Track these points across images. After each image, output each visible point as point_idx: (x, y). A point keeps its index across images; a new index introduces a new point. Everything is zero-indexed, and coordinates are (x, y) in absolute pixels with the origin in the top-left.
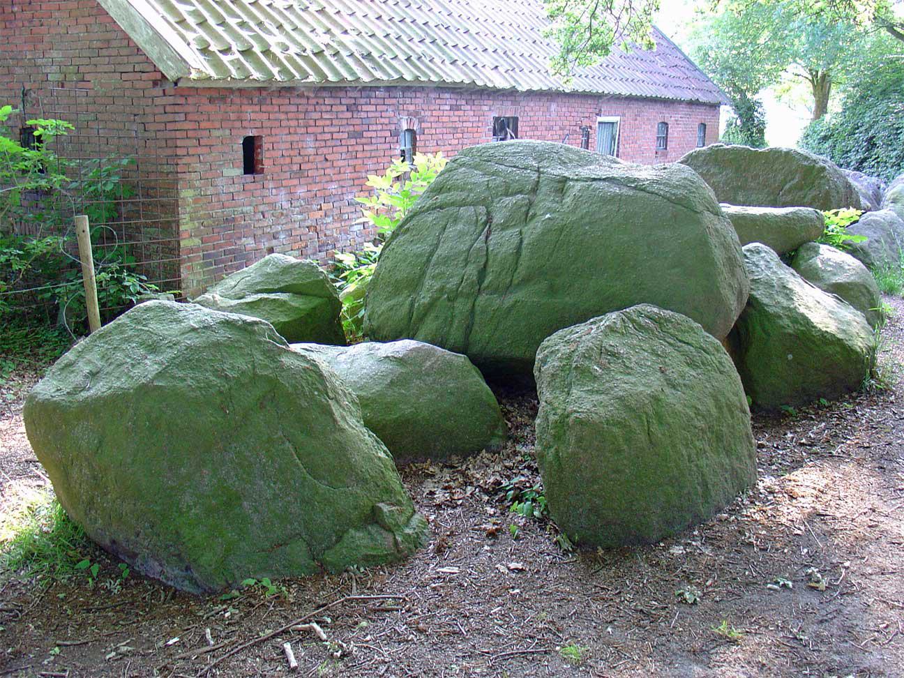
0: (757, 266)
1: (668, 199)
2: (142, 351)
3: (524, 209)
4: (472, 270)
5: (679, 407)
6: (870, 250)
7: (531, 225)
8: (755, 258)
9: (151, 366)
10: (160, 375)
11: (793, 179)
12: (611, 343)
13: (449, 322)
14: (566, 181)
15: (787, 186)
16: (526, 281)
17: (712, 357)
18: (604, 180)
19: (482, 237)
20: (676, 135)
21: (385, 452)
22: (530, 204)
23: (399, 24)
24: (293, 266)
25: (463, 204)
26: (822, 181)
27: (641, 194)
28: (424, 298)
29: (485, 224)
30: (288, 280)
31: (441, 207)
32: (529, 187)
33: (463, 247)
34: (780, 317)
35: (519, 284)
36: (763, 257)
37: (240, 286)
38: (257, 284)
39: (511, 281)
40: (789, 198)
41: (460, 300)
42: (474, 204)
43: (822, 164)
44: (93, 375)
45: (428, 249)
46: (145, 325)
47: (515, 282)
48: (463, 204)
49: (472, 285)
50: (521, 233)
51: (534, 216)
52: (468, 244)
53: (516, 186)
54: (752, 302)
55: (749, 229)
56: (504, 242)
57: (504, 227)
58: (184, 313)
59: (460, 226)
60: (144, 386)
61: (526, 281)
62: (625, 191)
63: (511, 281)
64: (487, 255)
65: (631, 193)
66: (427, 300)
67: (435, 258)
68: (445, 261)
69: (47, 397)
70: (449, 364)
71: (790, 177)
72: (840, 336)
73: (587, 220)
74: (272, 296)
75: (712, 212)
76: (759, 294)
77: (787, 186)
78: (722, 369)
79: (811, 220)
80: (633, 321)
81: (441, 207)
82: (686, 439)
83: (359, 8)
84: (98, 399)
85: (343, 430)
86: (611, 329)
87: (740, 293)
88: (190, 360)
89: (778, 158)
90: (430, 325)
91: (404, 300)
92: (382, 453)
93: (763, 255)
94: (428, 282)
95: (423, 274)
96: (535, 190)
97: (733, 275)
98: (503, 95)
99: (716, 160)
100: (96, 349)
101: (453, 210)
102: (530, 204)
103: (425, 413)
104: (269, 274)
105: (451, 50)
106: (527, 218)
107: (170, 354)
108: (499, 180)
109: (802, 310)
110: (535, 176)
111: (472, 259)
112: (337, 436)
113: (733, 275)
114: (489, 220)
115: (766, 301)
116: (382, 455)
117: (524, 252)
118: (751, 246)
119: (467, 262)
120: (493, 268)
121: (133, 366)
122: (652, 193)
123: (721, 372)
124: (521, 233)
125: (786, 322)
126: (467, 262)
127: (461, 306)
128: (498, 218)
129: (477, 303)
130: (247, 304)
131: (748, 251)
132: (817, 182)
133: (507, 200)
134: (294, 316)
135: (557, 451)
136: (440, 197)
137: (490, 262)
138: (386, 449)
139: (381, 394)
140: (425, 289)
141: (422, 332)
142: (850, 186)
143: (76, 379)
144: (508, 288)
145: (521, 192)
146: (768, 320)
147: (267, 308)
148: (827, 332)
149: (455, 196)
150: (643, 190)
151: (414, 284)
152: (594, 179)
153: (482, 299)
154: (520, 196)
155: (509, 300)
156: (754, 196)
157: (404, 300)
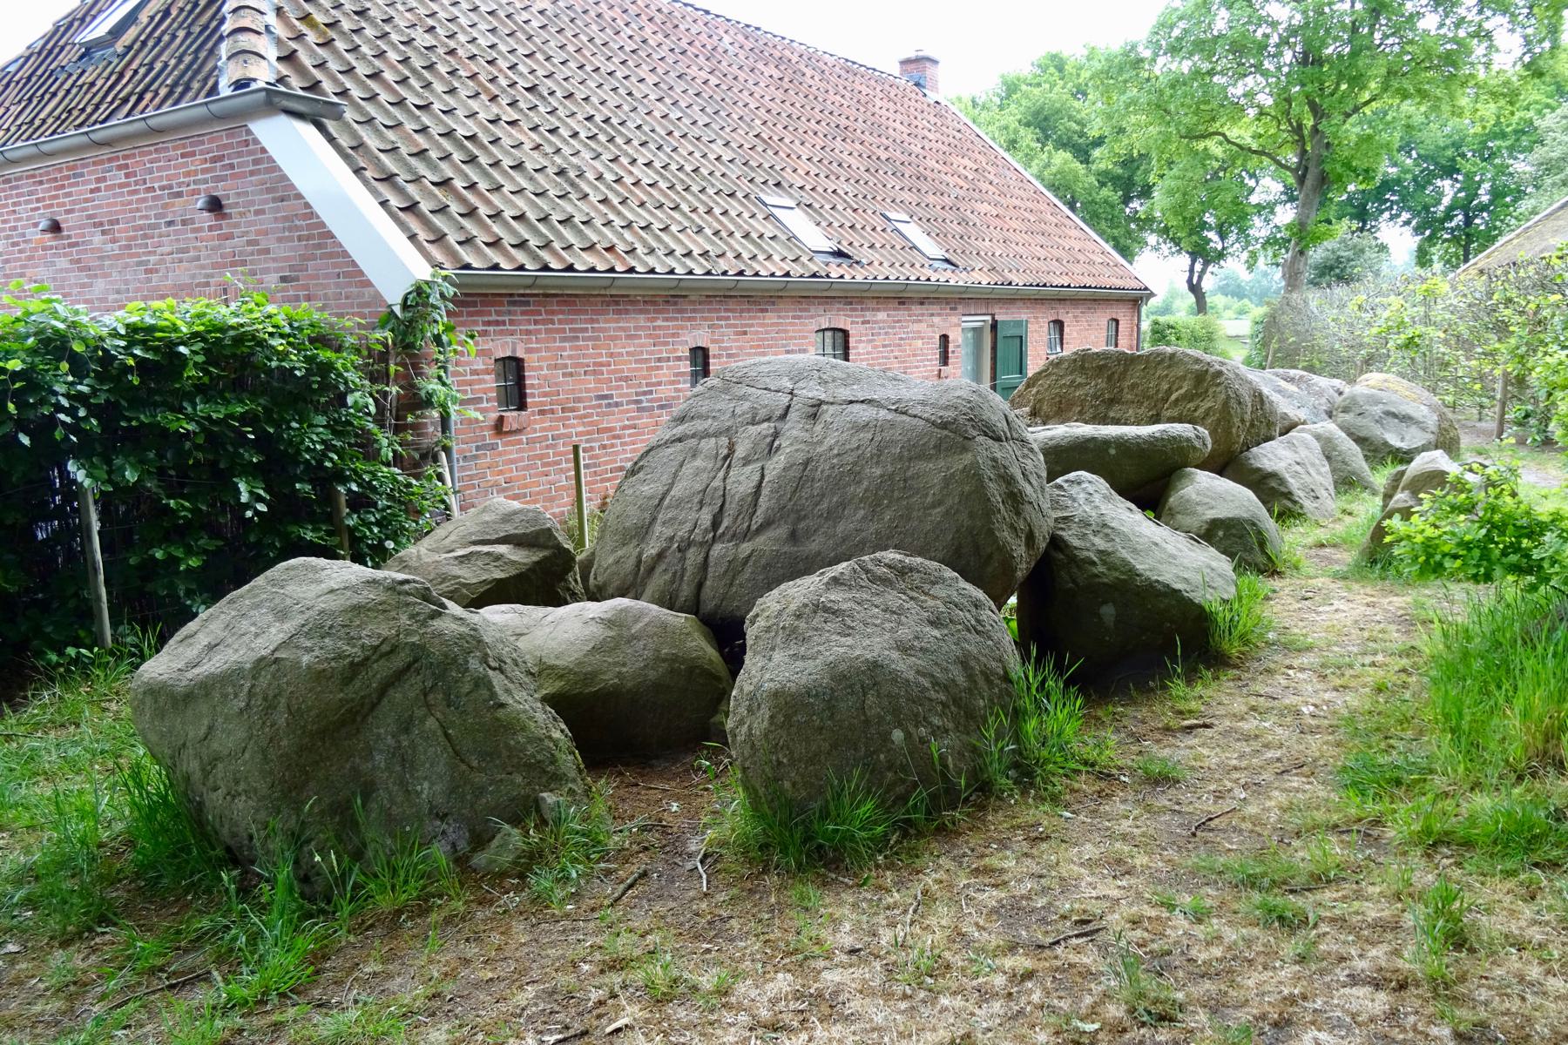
0: (1074, 500)
1: (934, 423)
2: (270, 617)
3: (769, 440)
4: (706, 518)
5: (911, 675)
6: (1287, 476)
7: (775, 459)
8: (1074, 490)
9: (276, 634)
10: (283, 645)
11: (1181, 388)
12: (832, 598)
13: (678, 577)
14: (819, 405)
15: (1173, 397)
16: (766, 525)
17: (967, 614)
18: (862, 402)
19: (721, 474)
20: (1075, 334)
21: (562, 731)
22: (776, 435)
23: (721, 217)
24: (515, 513)
25: (706, 435)
26: (1219, 389)
27: (904, 417)
28: (651, 550)
29: (726, 458)
30: (510, 529)
31: (680, 440)
32: (778, 413)
33: (698, 487)
34: (1094, 563)
35: (757, 529)
36: (1084, 489)
37: (452, 538)
38: (471, 534)
39: (749, 526)
40: (1175, 413)
41: (692, 550)
42: (716, 435)
43: (1217, 367)
44: (211, 647)
45: (661, 489)
46: (282, 587)
47: (754, 527)
48: (706, 435)
49: (706, 531)
50: (763, 468)
51: (778, 448)
52: (706, 482)
53: (762, 413)
54: (1056, 542)
55: (1063, 459)
56: (742, 480)
57: (747, 461)
58: (329, 571)
59: (698, 463)
60: (263, 658)
61: (766, 525)
62: (883, 413)
63: (749, 526)
64: (724, 495)
65: (890, 416)
66: (654, 552)
67: (667, 502)
68: (679, 503)
69: (153, 675)
70: (664, 626)
71: (1176, 386)
72: (1177, 586)
73: (835, 452)
74: (486, 549)
75: (991, 438)
76: (1070, 536)
77: (1173, 397)
78: (979, 628)
79: (1188, 440)
80: (867, 571)
81: (680, 440)
82: (916, 715)
83: (717, 203)
84: (212, 676)
85: (502, 705)
86: (835, 581)
87: (1030, 539)
88: (319, 629)
89: (1162, 360)
90: (658, 581)
91: (631, 551)
92: (559, 732)
93: (1084, 486)
94: (658, 528)
95: (654, 519)
96: (784, 416)
97: (1018, 514)
98: (947, 301)
99: (1082, 367)
100: (223, 616)
101: (693, 442)
102: (776, 435)
103: (630, 685)
104: (487, 523)
105: (769, 245)
106: (771, 450)
107: (300, 620)
108: (747, 405)
109: (1124, 554)
110: (785, 399)
111: (707, 500)
112: (501, 713)
113: (1018, 514)
114: (731, 449)
115: (1076, 542)
116: (557, 735)
117: (765, 491)
118: (1072, 475)
119: (701, 504)
120: (731, 509)
121: (257, 635)
122: (915, 416)
123: (978, 632)
124: (763, 468)
125: (1101, 569)
126: (701, 504)
127: (693, 556)
128: (740, 451)
129: (711, 553)
130: (456, 558)
131: (1067, 481)
132: (1211, 391)
133: (753, 430)
134: (513, 572)
135: (750, 728)
136: (681, 428)
137: (727, 505)
138: (563, 726)
139: (580, 664)
140: (654, 537)
141: (649, 591)
142: (1261, 395)
143: (191, 653)
144: (747, 535)
145: (768, 419)
146: (1078, 566)
147: (479, 563)
148: (1157, 581)
149: (700, 425)
150: (905, 413)
151: (642, 532)
152: (851, 402)
153: (717, 549)
154: (765, 425)
155: (746, 548)
156: (1131, 411)
157: (631, 551)
